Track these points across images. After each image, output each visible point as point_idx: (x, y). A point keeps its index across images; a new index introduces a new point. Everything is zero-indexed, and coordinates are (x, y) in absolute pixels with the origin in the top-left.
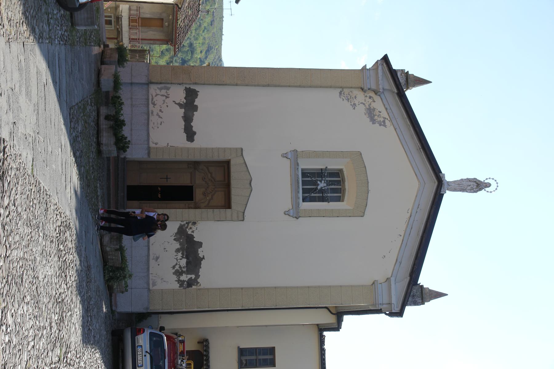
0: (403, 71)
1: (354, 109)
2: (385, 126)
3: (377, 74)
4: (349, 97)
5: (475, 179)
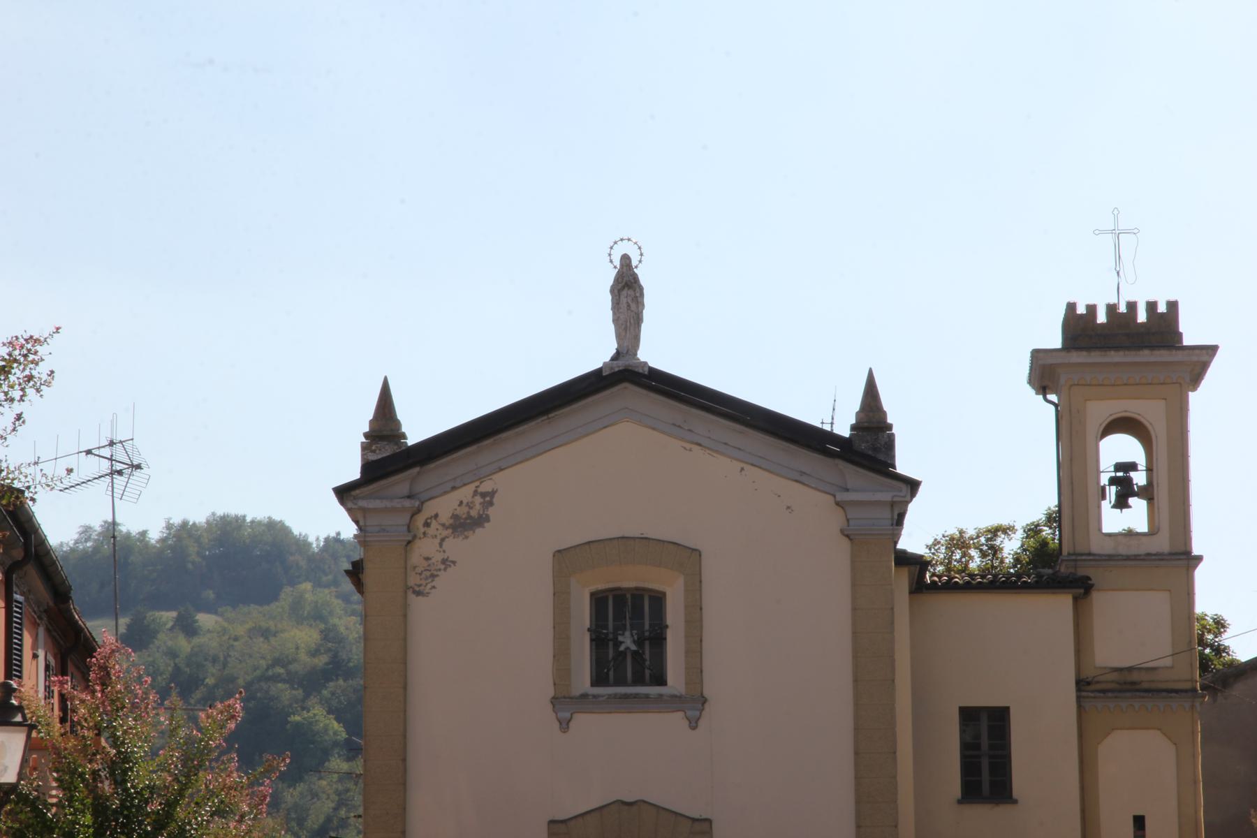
0: (365, 448)
1: (454, 563)
2: (492, 494)
3: (375, 510)
4: (428, 574)
5: (612, 291)
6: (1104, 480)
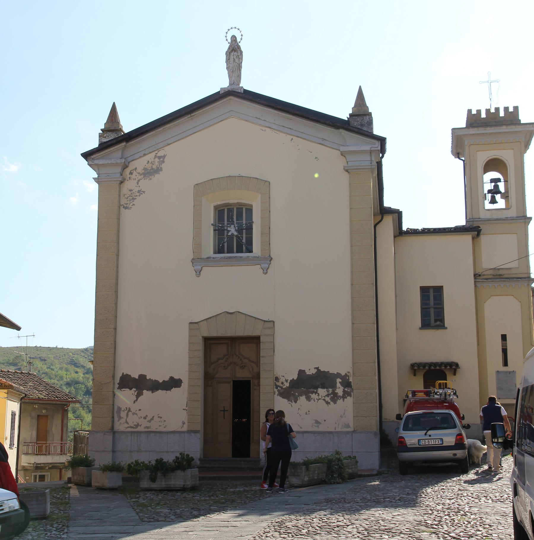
0: (100, 136)
1: (144, 192)
2: (164, 156)
3: (104, 165)
5: (226, 54)
6: (486, 191)
